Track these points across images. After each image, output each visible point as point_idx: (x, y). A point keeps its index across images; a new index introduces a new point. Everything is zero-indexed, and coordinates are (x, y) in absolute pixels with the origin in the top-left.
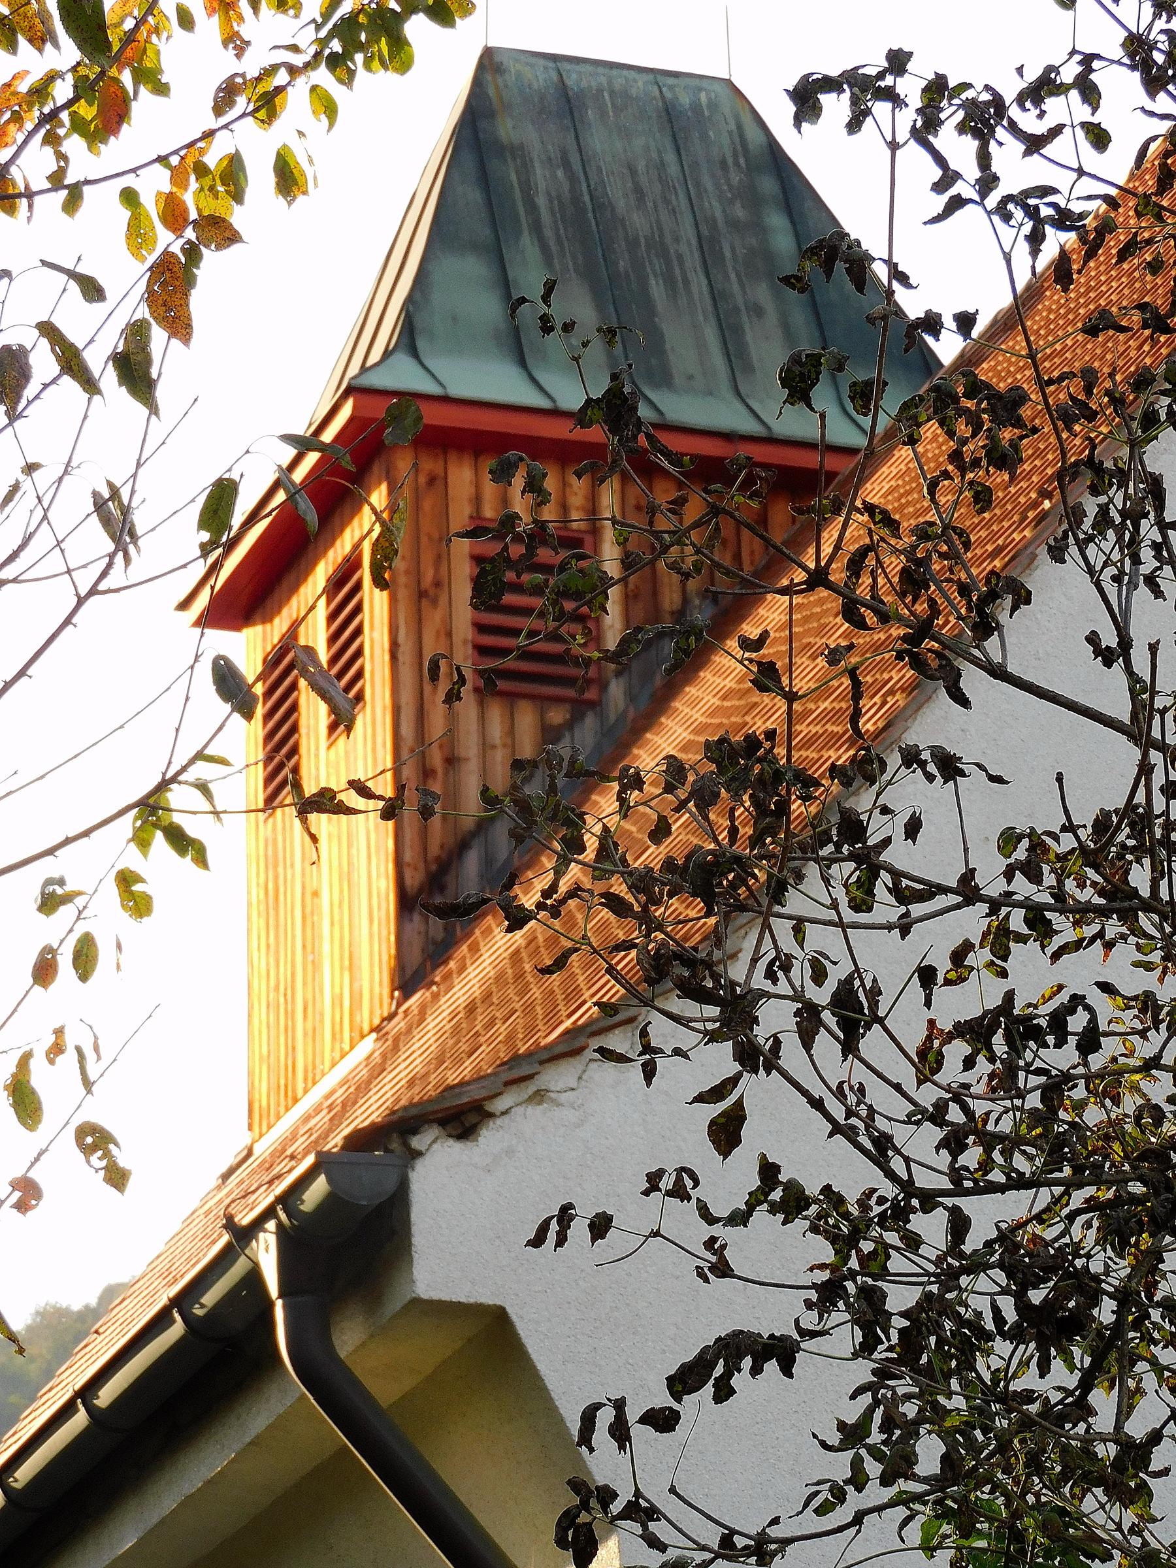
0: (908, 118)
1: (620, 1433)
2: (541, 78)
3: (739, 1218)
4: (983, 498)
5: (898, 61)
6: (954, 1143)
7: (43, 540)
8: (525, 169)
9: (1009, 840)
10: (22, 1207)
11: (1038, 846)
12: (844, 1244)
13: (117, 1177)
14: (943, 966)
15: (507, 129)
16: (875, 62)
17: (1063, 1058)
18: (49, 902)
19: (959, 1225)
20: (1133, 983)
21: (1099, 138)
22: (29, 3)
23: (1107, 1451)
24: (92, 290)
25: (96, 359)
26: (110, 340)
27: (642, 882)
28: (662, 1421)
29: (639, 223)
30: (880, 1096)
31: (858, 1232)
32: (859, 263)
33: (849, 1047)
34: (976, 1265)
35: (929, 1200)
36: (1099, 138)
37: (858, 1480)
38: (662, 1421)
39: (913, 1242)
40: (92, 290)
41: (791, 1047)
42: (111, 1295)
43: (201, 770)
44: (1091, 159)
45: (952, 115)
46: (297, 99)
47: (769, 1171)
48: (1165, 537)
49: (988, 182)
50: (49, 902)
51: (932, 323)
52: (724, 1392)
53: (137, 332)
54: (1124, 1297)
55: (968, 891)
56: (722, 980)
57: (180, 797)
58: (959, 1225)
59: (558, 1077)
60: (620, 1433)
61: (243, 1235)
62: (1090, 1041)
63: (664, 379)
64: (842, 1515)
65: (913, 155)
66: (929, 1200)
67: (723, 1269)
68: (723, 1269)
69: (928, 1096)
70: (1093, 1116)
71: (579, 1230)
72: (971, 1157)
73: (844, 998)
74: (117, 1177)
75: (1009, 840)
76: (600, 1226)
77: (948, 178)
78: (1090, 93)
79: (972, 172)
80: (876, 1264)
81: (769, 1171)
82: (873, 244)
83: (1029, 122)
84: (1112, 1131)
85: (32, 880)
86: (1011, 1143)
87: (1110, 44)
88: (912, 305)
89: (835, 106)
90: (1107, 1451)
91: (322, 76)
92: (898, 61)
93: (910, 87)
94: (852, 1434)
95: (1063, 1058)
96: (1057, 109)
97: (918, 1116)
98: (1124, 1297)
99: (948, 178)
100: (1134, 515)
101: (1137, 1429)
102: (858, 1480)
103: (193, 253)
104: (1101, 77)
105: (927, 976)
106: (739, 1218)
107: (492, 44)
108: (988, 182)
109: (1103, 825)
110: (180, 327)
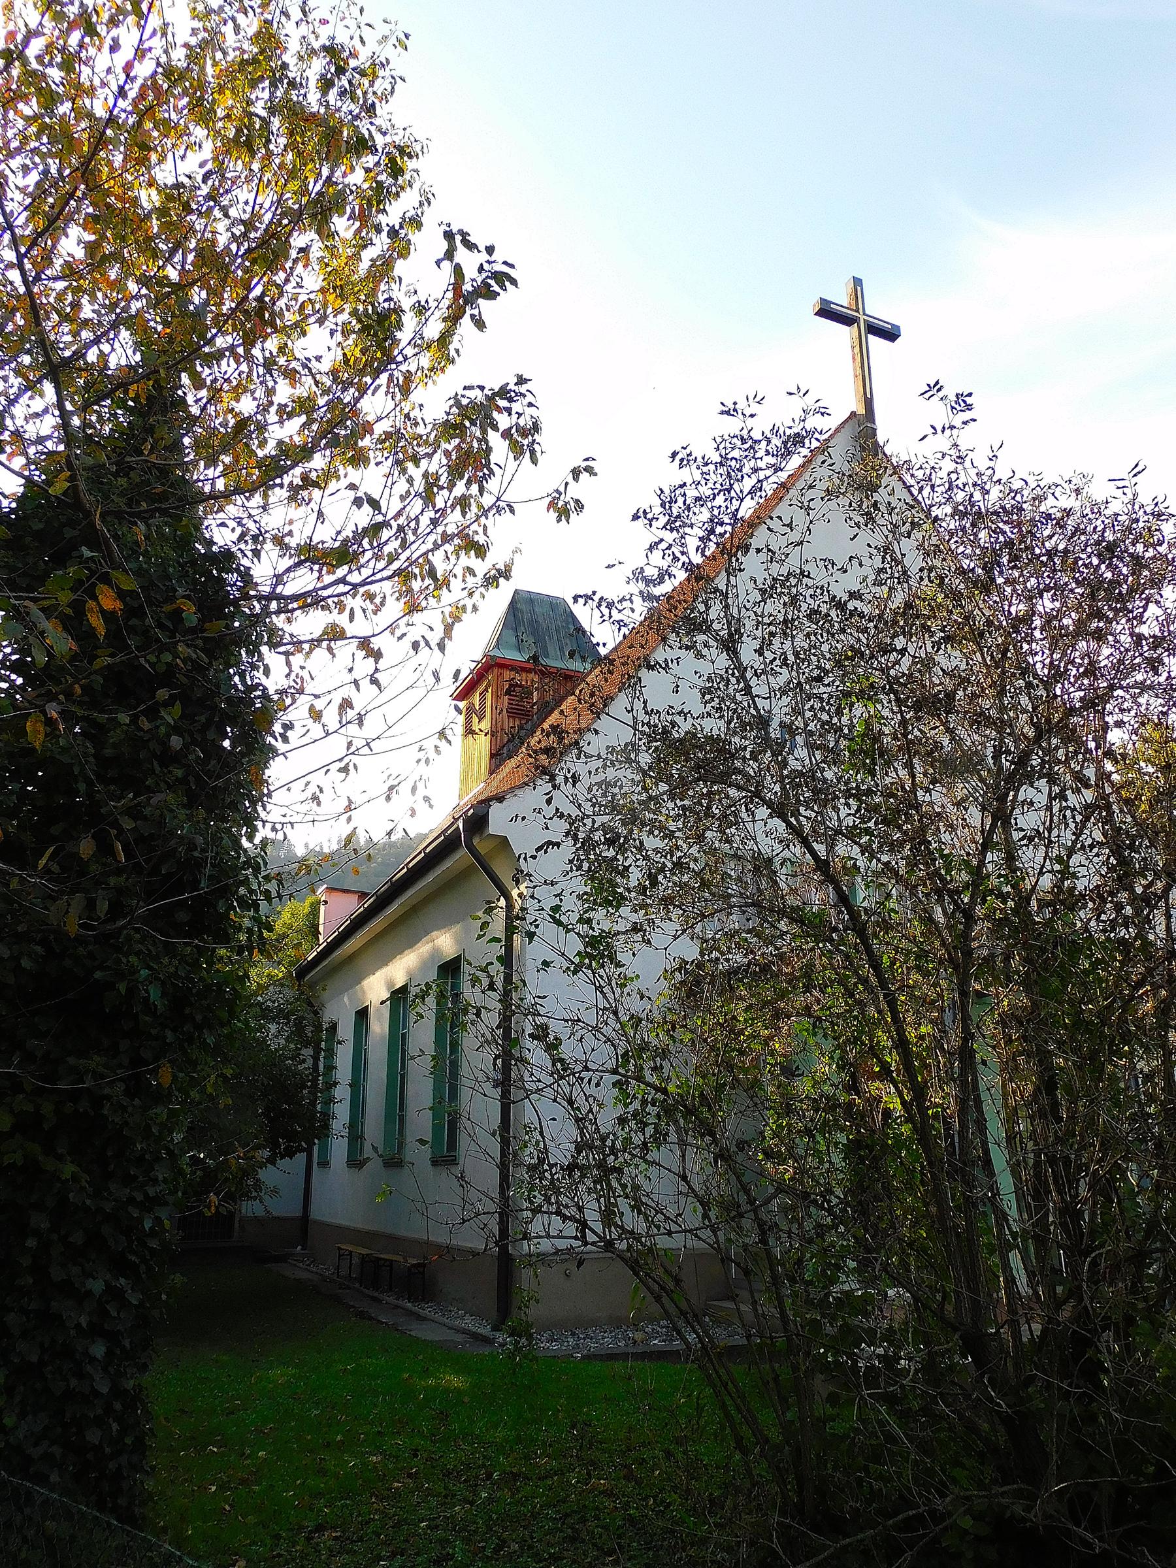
0: (595, 603)
1: (525, 859)
2: (526, 595)
3: (551, 818)
4: (606, 680)
5: (594, 593)
6: (594, 806)
7: (421, 680)
8: (522, 613)
9: (608, 747)
10: (412, 816)
11: (613, 749)
12: (571, 824)
13: (431, 806)
14: (593, 771)
15: (519, 605)
16: (590, 593)
17: (616, 790)
18: (420, 749)
19: (594, 822)
20: (631, 776)
21: (633, 610)
22: (72, 3)
23: (621, 868)
24: (431, 629)
25: (433, 644)
26: (437, 640)
27: (535, 752)
28: (534, 857)
29: (545, 626)
30: (580, 796)
31: (574, 822)
32: (584, 632)
33: (574, 786)
34: (597, 830)
35: (588, 817)
36: (633, 610)
37: (571, 870)
38: (534, 857)
39: (585, 825)
40: (431, 629)
41: (563, 784)
42: (431, 831)
43: (452, 725)
44: (631, 614)
45: (604, 604)
46: (477, 595)
47: (557, 810)
48: (490, 508)
49: (610, 617)
50: (420, 749)
51: (598, 644)
52: (546, 852)
53: (442, 639)
54: (625, 837)
55: (599, 756)
56: (267, 315)
57: (448, 732)
58: (594, 822)
59: (520, 791)
60: (525, 859)
61: (456, 820)
62: (621, 787)
63: (547, 657)
64: (568, 877)
65: (596, 611)
66: (588, 817)
67: (547, 828)
68: (547, 828)
69: (589, 796)
70: (621, 802)
71: (520, 819)
72: (597, 809)
73: (573, 776)
74: (431, 806)
75: (608, 747)
76: (524, 818)
77: (603, 616)
78: (632, 602)
79: (607, 615)
80: (577, 829)
81: (557, 810)
82: (587, 628)
83: (620, 607)
84: (624, 806)
85: (417, 746)
86: (606, 807)
87: (636, 592)
88: (594, 641)
89: (581, 601)
90: (621, 868)
91: (482, 589)
92: (594, 593)
93: (596, 598)
94: (571, 862)
95: (616, 790)
96: (627, 604)
97: (587, 800)
98: (625, 837)
99: (603, 616)
100: (635, 684)
101: (626, 864)
102: (571, 870)
103: (453, 623)
104: (634, 598)
105: (590, 772)
106: (551, 818)
107: (519, 588)
108: (610, 617)
109: (626, 745)
110: (450, 638)
